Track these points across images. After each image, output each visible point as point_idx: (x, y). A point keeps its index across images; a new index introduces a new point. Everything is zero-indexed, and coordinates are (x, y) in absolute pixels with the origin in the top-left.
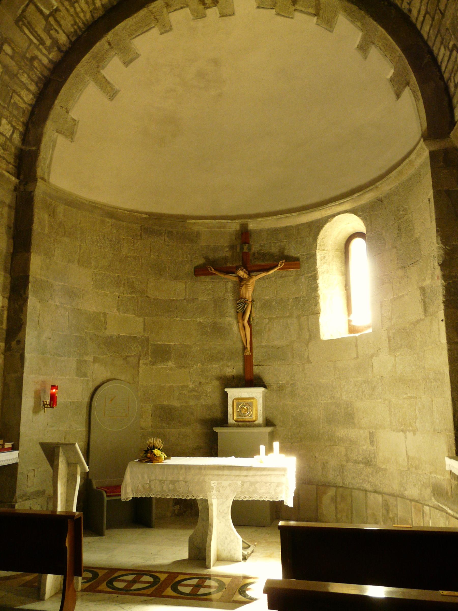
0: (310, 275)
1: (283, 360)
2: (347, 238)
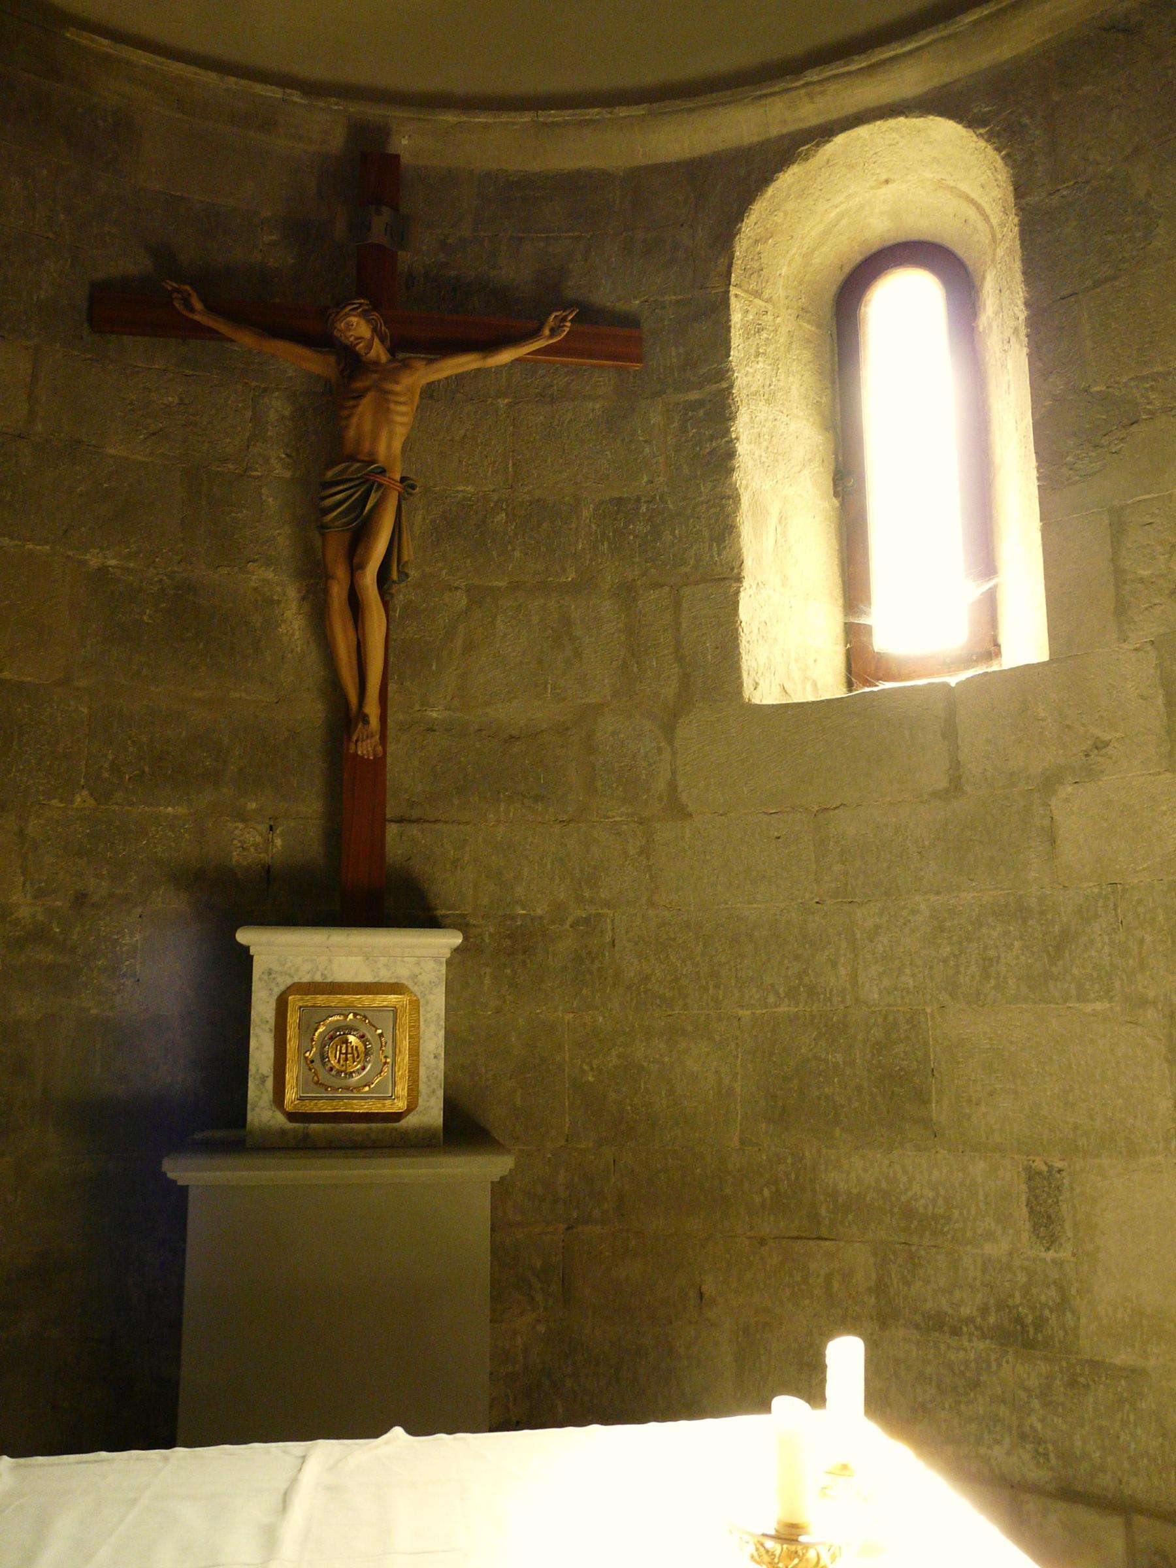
0: (693, 396)
1: (536, 798)
2: (848, 269)
